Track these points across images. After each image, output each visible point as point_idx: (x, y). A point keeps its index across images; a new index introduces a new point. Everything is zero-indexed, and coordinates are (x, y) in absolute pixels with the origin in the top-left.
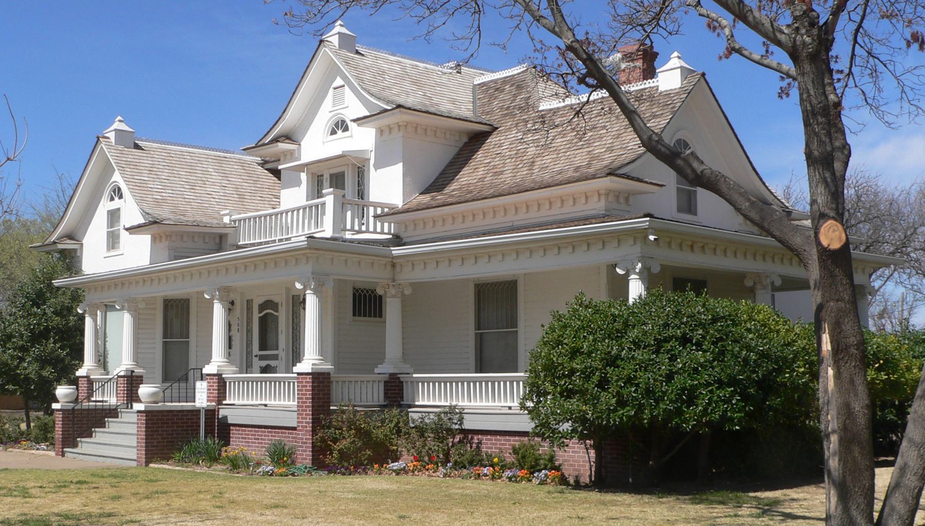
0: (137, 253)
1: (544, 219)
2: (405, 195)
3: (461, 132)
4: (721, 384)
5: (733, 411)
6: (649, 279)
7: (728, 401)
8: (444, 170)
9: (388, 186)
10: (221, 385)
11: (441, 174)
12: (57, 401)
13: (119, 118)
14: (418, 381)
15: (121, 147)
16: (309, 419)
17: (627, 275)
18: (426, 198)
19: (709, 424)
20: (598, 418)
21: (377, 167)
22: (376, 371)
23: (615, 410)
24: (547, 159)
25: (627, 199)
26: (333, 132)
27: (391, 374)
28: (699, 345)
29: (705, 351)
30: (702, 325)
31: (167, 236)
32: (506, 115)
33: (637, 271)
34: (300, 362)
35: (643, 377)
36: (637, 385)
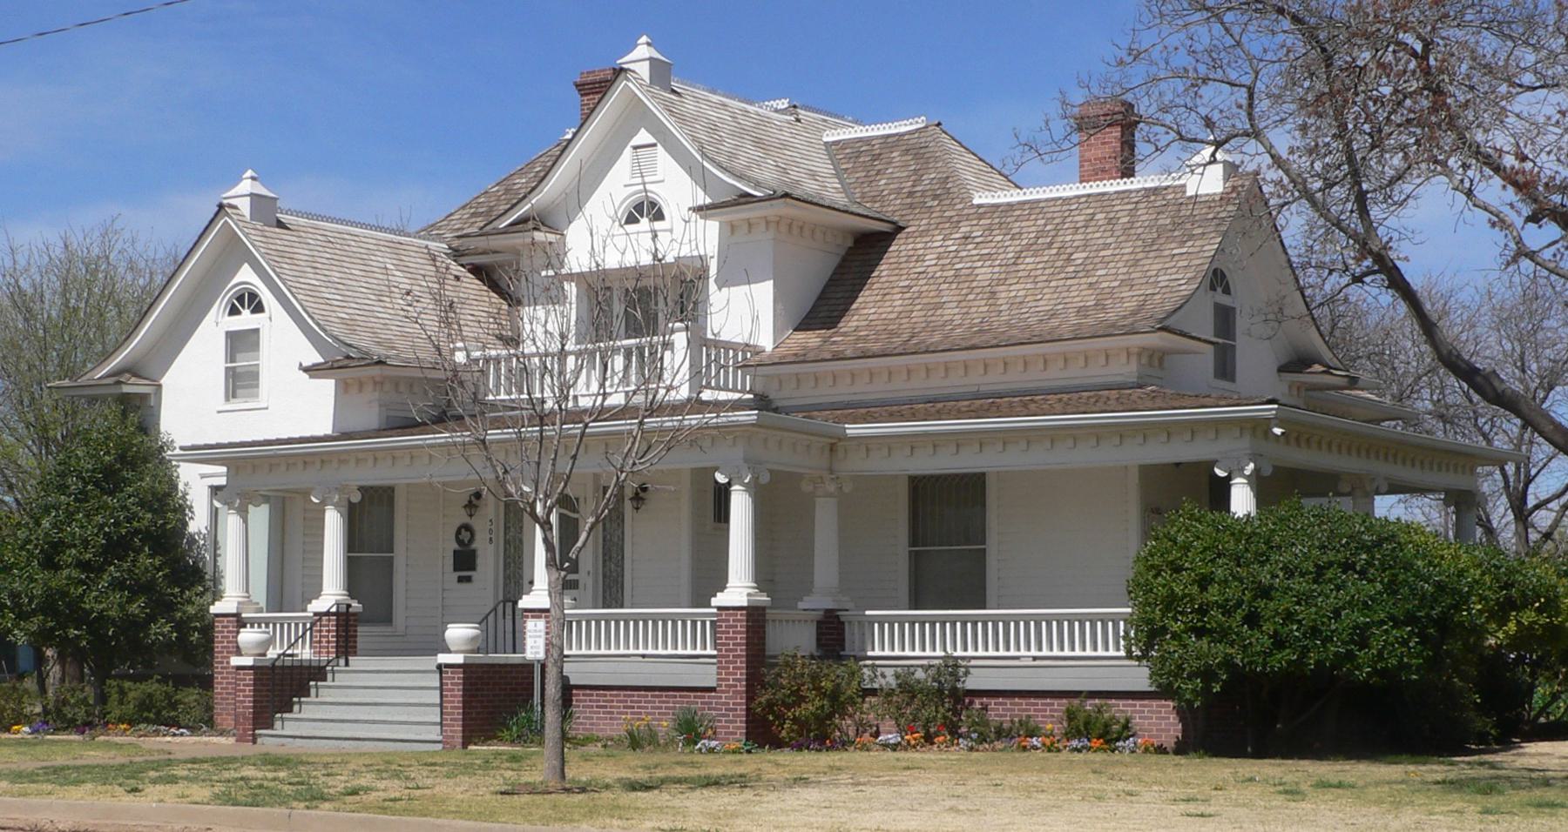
0: (298, 405)
1: (1031, 385)
2: (777, 331)
3: (846, 231)
4: (1397, 624)
5: (1410, 656)
6: (1260, 485)
7: (1405, 643)
8: (823, 292)
9: (746, 314)
10: (560, 627)
11: (820, 298)
12: (238, 652)
13: (249, 173)
14: (872, 621)
15: (259, 225)
16: (741, 674)
17: (1229, 478)
18: (812, 339)
19: (1383, 673)
20: (1251, 663)
21: (722, 283)
22: (801, 605)
23: (1271, 654)
24: (1018, 290)
25: (1161, 360)
26: (631, 219)
27: (827, 611)
28: (1363, 573)
29: (1370, 581)
30: (1364, 547)
31: (375, 383)
32: (911, 206)
33: (1247, 472)
34: (722, 590)
35: (1304, 613)
36: (1299, 622)
